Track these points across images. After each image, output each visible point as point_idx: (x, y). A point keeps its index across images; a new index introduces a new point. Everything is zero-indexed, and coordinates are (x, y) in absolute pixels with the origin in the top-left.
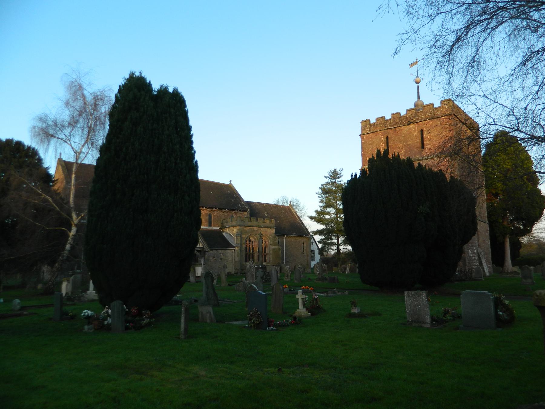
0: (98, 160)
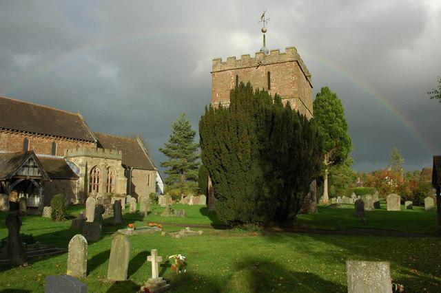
0: (373, 255)
